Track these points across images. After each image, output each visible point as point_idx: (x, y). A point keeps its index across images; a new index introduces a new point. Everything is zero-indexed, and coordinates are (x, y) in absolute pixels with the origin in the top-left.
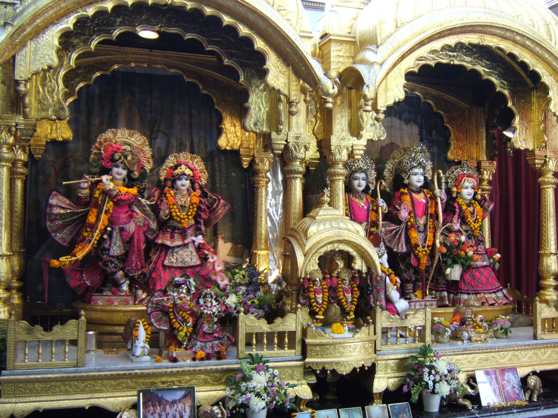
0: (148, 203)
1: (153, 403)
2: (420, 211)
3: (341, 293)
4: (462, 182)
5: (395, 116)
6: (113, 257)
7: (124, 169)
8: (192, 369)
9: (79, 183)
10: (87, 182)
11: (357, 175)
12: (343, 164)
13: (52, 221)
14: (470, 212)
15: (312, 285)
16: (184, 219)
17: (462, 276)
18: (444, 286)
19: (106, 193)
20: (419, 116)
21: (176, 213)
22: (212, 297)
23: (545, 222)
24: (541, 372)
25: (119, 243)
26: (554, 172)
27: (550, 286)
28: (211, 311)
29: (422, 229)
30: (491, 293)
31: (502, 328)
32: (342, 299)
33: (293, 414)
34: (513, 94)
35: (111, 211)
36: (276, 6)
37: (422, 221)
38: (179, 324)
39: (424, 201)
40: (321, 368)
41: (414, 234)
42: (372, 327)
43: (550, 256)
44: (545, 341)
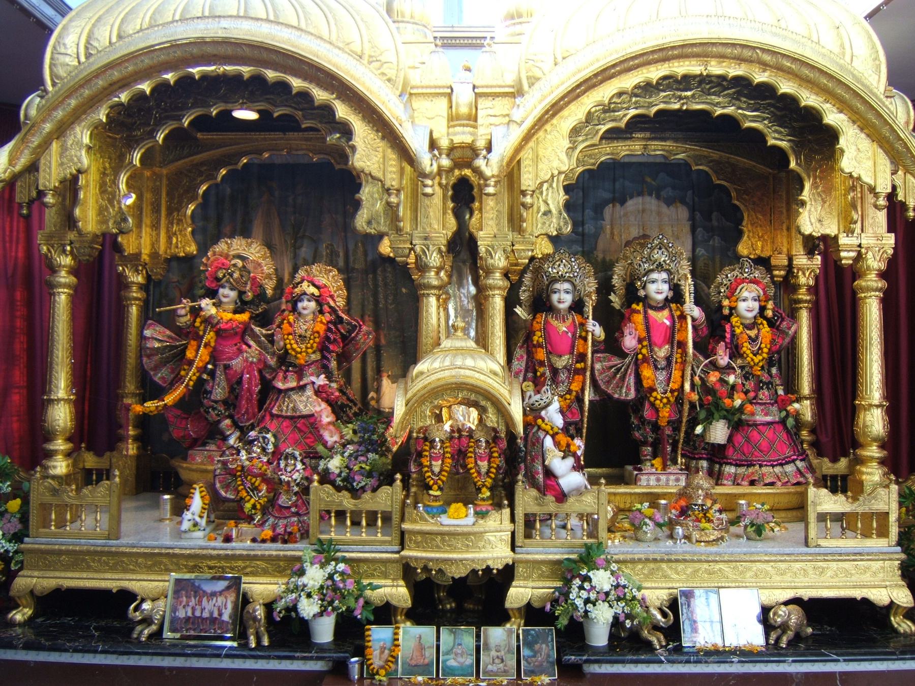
0: (264, 332)
1: (187, 592)
2: (657, 337)
3: (472, 460)
4: (738, 291)
5: (650, 195)
6: (216, 402)
7: (232, 289)
8: (245, 553)
9: (177, 309)
10: (184, 308)
11: (557, 286)
12: (501, 273)
13: (149, 356)
14: (750, 337)
15: (427, 448)
16: (301, 353)
17: (730, 439)
18: (703, 451)
19: (208, 321)
20: (690, 193)
21: (291, 344)
22: (296, 459)
23: (862, 354)
24: (812, 600)
25: (224, 384)
26: (879, 270)
27: (872, 458)
28: (291, 477)
29: (663, 363)
30: (773, 466)
31: (752, 524)
32: (471, 468)
33: (367, 627)
34: (799, 147)
35: (213, 344)
36: (366, 57)
37: (662, 353)
38: (248, 492)
39: (668, 323)
40: (422, 565)
41: (647, 372)
42: (507, 512)
43: (869, 410)
44: (822, 550)
